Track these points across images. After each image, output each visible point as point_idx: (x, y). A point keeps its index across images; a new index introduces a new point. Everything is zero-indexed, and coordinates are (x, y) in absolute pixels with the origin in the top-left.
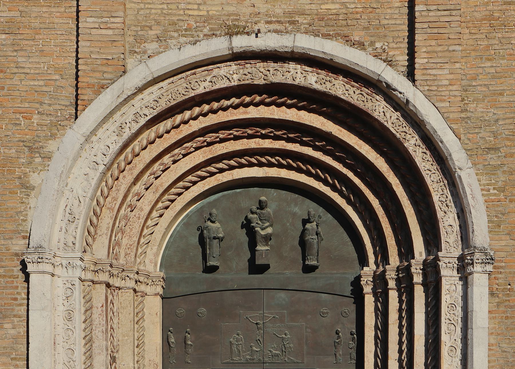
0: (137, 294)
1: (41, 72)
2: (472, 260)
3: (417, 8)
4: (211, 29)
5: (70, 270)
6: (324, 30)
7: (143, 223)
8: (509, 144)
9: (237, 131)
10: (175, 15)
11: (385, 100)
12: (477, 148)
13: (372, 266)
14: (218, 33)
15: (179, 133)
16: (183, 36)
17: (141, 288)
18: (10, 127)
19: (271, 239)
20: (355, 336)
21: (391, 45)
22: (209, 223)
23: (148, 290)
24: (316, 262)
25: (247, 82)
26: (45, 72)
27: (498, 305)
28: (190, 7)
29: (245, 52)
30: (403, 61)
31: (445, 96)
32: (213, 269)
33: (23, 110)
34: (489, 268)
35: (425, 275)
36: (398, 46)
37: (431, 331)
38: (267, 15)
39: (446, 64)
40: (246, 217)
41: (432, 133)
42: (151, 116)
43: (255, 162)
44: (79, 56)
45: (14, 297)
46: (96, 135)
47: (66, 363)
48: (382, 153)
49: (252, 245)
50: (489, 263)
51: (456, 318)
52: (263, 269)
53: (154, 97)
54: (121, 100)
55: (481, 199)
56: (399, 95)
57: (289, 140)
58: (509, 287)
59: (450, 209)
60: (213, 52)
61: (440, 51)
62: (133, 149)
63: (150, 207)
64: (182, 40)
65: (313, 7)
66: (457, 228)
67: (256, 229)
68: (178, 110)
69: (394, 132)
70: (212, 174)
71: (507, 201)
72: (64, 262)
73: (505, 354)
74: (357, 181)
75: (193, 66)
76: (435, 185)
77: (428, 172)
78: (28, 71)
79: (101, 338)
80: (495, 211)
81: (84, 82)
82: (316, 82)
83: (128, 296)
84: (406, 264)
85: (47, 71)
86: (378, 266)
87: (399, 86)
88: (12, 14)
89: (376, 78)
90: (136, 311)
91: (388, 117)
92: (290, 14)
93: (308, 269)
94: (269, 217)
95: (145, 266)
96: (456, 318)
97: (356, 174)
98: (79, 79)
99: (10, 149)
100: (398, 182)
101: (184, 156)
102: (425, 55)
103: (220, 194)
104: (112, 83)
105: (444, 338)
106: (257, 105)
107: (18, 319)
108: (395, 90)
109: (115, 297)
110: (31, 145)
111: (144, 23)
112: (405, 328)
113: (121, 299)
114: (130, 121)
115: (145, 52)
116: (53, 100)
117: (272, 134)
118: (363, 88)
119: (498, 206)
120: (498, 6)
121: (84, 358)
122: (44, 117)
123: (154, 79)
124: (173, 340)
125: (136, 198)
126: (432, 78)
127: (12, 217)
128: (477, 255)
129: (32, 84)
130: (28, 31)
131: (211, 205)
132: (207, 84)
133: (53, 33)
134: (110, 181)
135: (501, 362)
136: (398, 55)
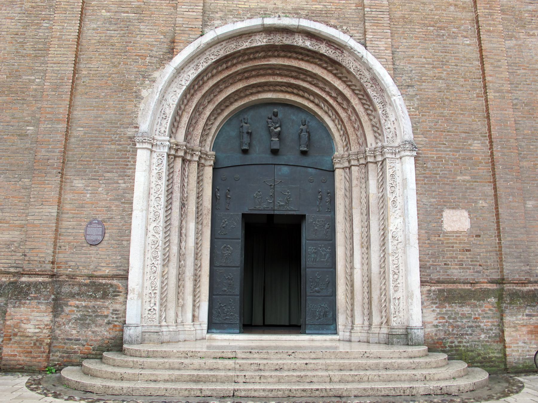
4: (251, 15)
5: (162, 148)
10: (231, 7)
18: (132, 63)
21: (351, 28)
28: (239, 3)
56: (358, 54)
88: (139, 3)
107: (128, 178)
115: (213, 25)
122: (153, 58)
132: (247, 44)
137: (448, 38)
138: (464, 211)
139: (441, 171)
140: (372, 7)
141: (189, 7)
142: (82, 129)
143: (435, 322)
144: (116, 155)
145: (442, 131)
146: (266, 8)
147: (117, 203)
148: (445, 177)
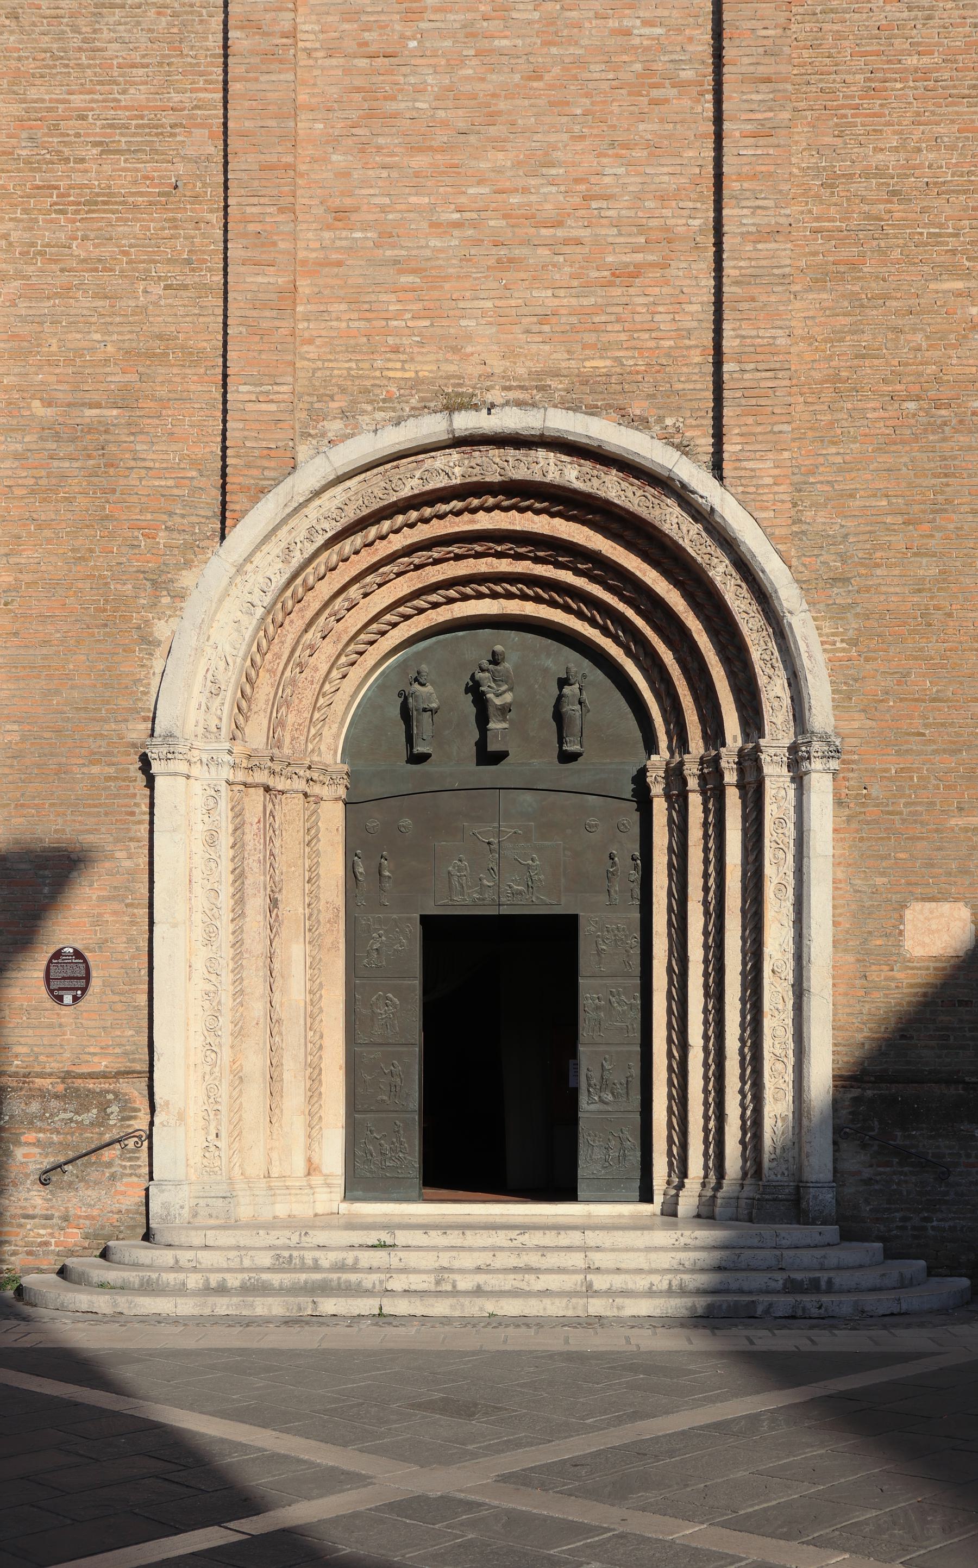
0: (309, 799)
1: (170, 466)
2: (808, 752)
3: (726, 367)
4: (422, 399)
5: (213, 769)
6: (589, 400)
7: (317, 690)
8: (864, 572)
9: (459, 548)
10: (368, 377)
11: (679, 505)
12: (816, 579)
13: (665, 753)
14: (432, 404)
15: (373, 553)
16: (380, 409)
17: (316, 789)
18: (124, 550)
19: (510, 711)
20: (639, 862)
21: (688, 421)
22: (416, 686)
23: (325, 792)
24: (578, 747)
25: (474, 479)
26: (176, 466)
27: (849, 820)
28: (390, 365)
29: (471, 436)
30: (705, 446)
31: (767, 501)
32: (421, 758)
33: (144, 524)
34: (834, 764)
35: (741, 771)
36: (698, 422)
37: (751, 858)
38: (503, 377)
39: (768, 453)
40: (473, 675)
41: (749, 557)
42: (333, 532)
43: (486, 591)
44: (228, 444)
45: (129, 810)
46: (251, 562)
47: (207, 912)
48: (677, 584)
49: (482, 719)
50: (833, 757)
51: (786, 840)
52: (499, 757)
53: (337, 502)
54: (290, 509)
55: (820, 657)
56: (700, 500)
57: (537, 560)
58: (865, 791)
59: (777, 672)
60: (425, 436)
61: (760, 433)
62: (305, 581)
63: (329, 665)
64: (379, 415)
65: (573, 364)
66: (787, 701)
67: (488, 696)
68: (372, 520)
69: (693, 554)
70: (421, 611)
71: (862, 659)
72: (205, 757)
73: (858, 895)
74: (639, 622)
75: (396, 456)
76: (755, 635)
77: (745, 615)
78: (151, 464)
79: (257, 871)
80: (844, 675)
81: (234, 484)
82: (577, 478)
83: (295, 804)
84: (713, 753)
85: (178, 464)
86: (672, 756)
87: (700, 486)
88: (128, 377)
89: (666, 474)
90: (308, 825)
91: (685, 531)
92: (539, 375)
93: (567, 758)
94: (507, 677)
95: (320, 754)
96: (786, 840)
97: (639, 612)
98: (228, 479)
99: (125, 584)
100: (700, 627)
101: (380, 586)
102: (738, 439)
103: (434, 639)
104: (277, 485)
105: (769, 870)
106: (489, 510)
107: (136, 844)
108: (693, 492)
109: (277, 807)
110: (155, 577)
111: (322, 391)
112: (712, 853)
113: (286, 809)
114: (302, 539)
115: (323, 435)
116: (188, 508)
117: (512, 552)
118: (647, 488)
119: (848, 667)
120: (847, 361)
121: (232, 902)
122: (175, 535)
123: (338, 477)
124: (361, 870)
125: (308, 652)
126: (748, 473)
127: (127, 687)
128: (816, 745)
129: (157, 484)
130: (152, 404)
131: (419, 656)
132: (415, 482)
133: (188, 406)
134: (271, 629)
135: (853, 907)
136: (699, 436)
137: (956, 431)
138: (961, 904)
139: (906, 804)
140: (744, 358)
141: (258, 389)
142: (16, 727)
143: (867, 1173)
144: (105, 789)
145: (916, 700)
146: (460, 377)
147: (117, 906)
148: (916, 821)
